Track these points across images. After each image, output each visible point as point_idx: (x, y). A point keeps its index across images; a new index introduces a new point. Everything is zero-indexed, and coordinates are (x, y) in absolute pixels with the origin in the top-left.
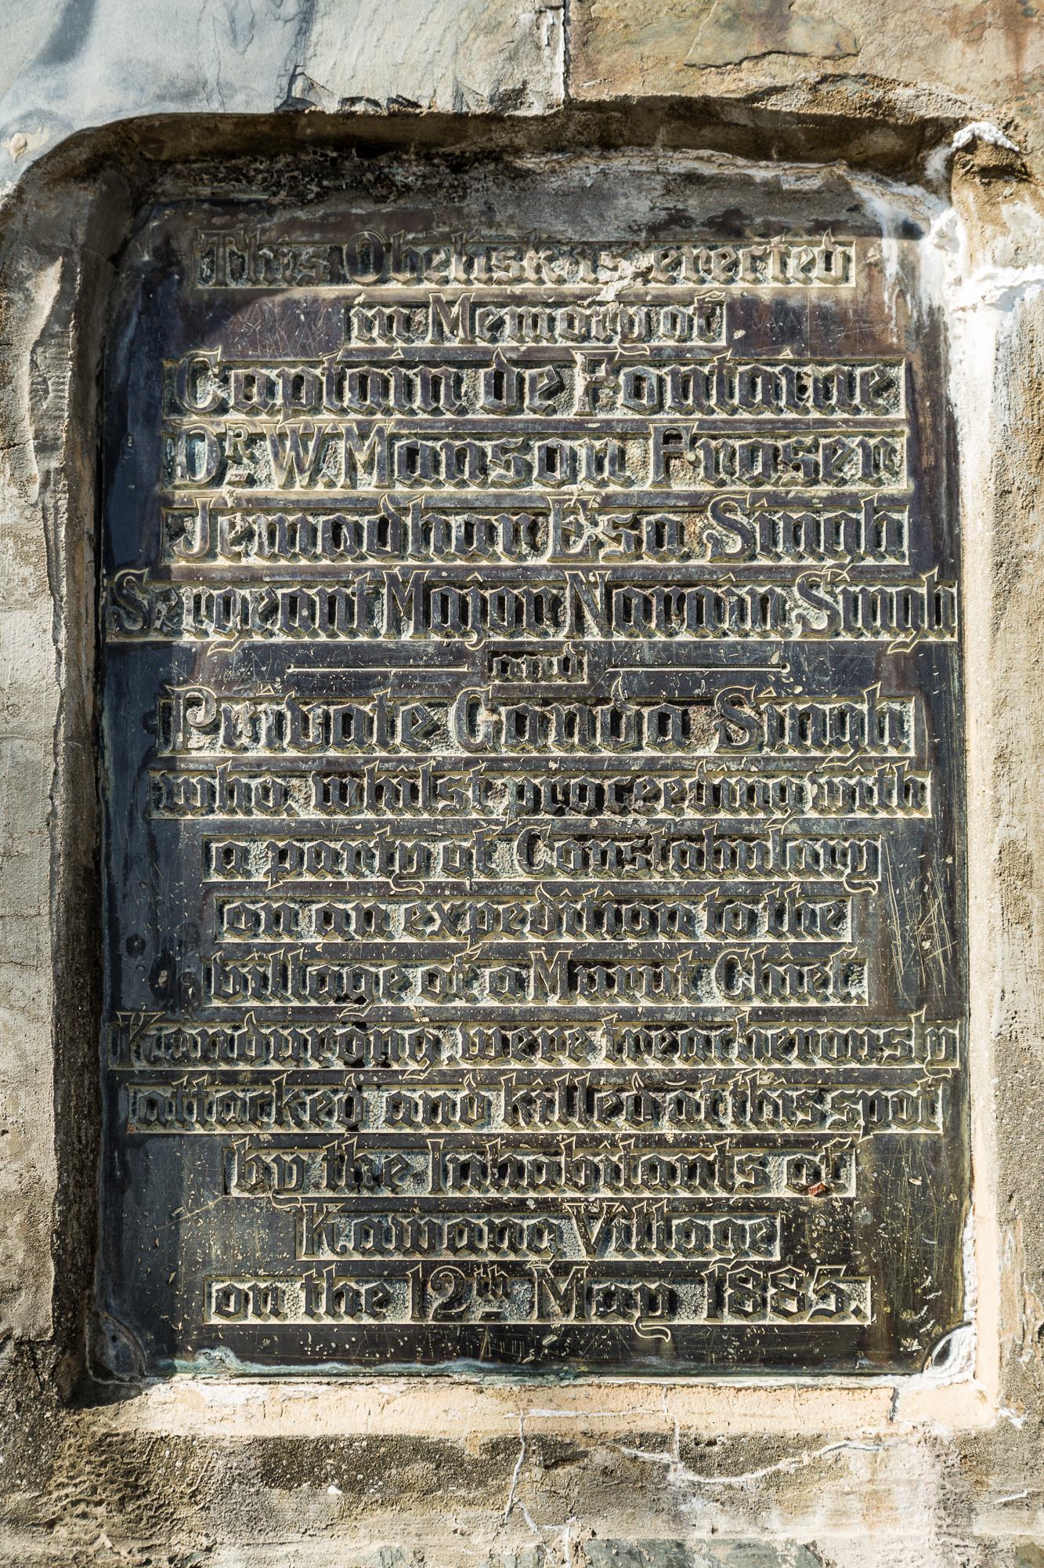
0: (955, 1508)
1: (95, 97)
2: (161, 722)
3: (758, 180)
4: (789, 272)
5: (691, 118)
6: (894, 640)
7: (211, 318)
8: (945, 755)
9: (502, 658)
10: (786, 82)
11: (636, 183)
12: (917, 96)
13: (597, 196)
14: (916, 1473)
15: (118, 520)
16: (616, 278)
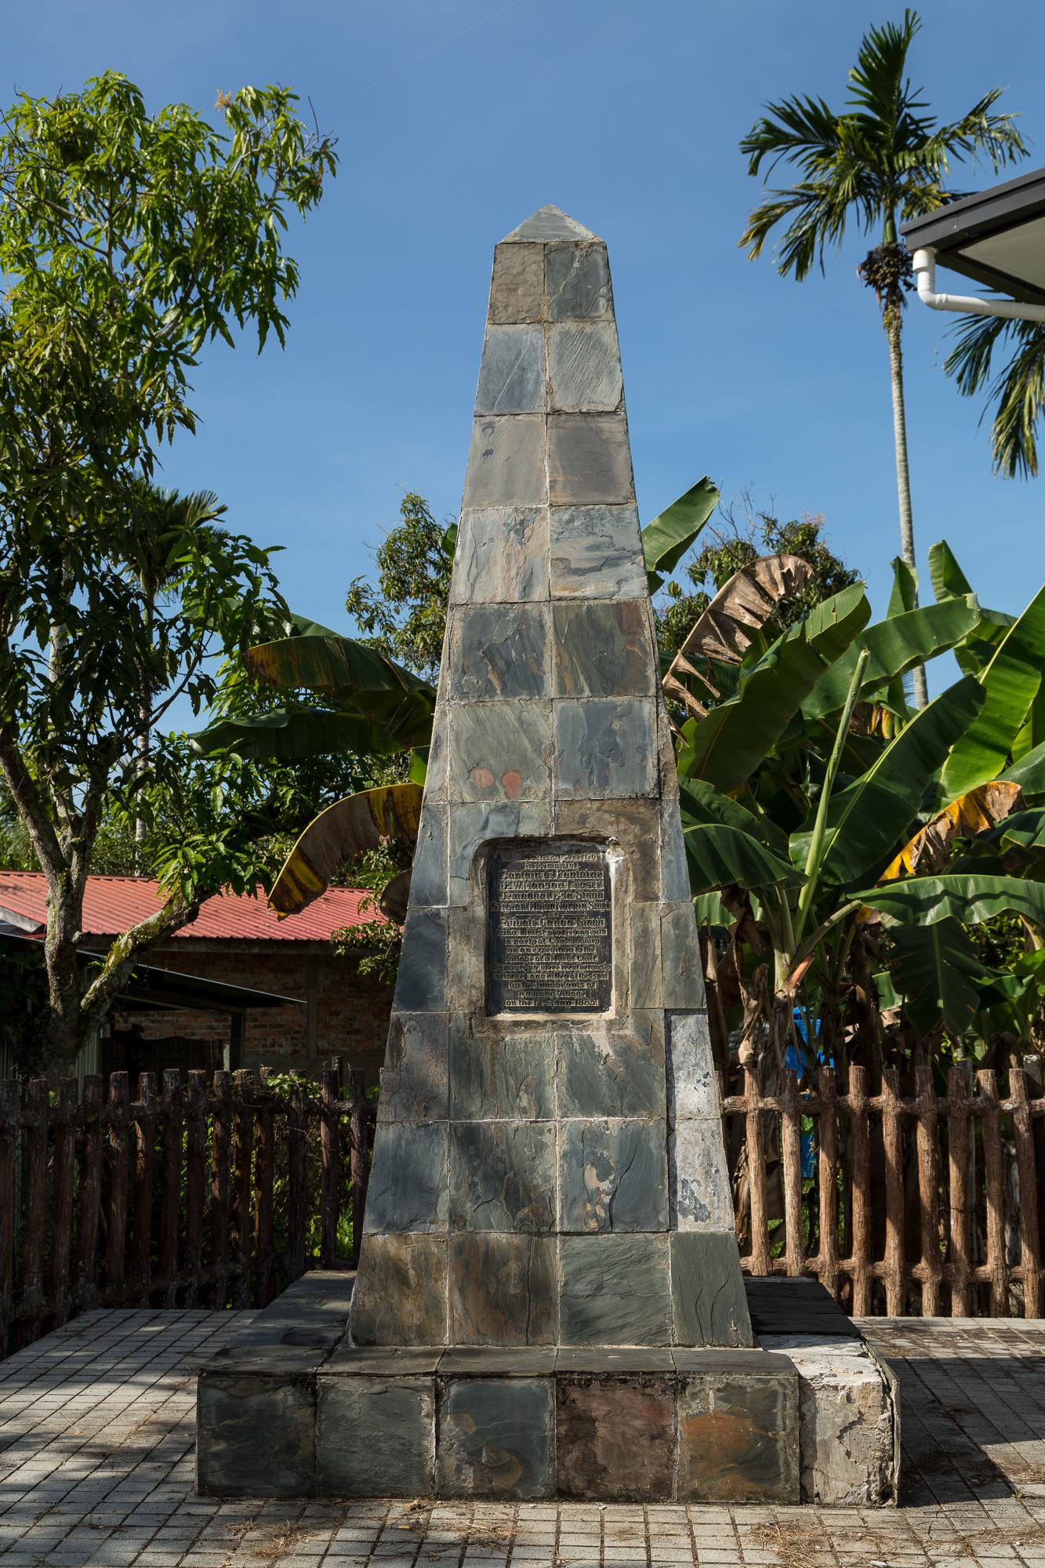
0: (609, 1030)
1: (489, 835)
2: (499, 922)
3: (425, 1443)
5: (573, 837)
6: (602, 910)
7: (504, 866)
8: (609, 926)
9: (546, 913)
10: (585, 831)
11: (565, 845)
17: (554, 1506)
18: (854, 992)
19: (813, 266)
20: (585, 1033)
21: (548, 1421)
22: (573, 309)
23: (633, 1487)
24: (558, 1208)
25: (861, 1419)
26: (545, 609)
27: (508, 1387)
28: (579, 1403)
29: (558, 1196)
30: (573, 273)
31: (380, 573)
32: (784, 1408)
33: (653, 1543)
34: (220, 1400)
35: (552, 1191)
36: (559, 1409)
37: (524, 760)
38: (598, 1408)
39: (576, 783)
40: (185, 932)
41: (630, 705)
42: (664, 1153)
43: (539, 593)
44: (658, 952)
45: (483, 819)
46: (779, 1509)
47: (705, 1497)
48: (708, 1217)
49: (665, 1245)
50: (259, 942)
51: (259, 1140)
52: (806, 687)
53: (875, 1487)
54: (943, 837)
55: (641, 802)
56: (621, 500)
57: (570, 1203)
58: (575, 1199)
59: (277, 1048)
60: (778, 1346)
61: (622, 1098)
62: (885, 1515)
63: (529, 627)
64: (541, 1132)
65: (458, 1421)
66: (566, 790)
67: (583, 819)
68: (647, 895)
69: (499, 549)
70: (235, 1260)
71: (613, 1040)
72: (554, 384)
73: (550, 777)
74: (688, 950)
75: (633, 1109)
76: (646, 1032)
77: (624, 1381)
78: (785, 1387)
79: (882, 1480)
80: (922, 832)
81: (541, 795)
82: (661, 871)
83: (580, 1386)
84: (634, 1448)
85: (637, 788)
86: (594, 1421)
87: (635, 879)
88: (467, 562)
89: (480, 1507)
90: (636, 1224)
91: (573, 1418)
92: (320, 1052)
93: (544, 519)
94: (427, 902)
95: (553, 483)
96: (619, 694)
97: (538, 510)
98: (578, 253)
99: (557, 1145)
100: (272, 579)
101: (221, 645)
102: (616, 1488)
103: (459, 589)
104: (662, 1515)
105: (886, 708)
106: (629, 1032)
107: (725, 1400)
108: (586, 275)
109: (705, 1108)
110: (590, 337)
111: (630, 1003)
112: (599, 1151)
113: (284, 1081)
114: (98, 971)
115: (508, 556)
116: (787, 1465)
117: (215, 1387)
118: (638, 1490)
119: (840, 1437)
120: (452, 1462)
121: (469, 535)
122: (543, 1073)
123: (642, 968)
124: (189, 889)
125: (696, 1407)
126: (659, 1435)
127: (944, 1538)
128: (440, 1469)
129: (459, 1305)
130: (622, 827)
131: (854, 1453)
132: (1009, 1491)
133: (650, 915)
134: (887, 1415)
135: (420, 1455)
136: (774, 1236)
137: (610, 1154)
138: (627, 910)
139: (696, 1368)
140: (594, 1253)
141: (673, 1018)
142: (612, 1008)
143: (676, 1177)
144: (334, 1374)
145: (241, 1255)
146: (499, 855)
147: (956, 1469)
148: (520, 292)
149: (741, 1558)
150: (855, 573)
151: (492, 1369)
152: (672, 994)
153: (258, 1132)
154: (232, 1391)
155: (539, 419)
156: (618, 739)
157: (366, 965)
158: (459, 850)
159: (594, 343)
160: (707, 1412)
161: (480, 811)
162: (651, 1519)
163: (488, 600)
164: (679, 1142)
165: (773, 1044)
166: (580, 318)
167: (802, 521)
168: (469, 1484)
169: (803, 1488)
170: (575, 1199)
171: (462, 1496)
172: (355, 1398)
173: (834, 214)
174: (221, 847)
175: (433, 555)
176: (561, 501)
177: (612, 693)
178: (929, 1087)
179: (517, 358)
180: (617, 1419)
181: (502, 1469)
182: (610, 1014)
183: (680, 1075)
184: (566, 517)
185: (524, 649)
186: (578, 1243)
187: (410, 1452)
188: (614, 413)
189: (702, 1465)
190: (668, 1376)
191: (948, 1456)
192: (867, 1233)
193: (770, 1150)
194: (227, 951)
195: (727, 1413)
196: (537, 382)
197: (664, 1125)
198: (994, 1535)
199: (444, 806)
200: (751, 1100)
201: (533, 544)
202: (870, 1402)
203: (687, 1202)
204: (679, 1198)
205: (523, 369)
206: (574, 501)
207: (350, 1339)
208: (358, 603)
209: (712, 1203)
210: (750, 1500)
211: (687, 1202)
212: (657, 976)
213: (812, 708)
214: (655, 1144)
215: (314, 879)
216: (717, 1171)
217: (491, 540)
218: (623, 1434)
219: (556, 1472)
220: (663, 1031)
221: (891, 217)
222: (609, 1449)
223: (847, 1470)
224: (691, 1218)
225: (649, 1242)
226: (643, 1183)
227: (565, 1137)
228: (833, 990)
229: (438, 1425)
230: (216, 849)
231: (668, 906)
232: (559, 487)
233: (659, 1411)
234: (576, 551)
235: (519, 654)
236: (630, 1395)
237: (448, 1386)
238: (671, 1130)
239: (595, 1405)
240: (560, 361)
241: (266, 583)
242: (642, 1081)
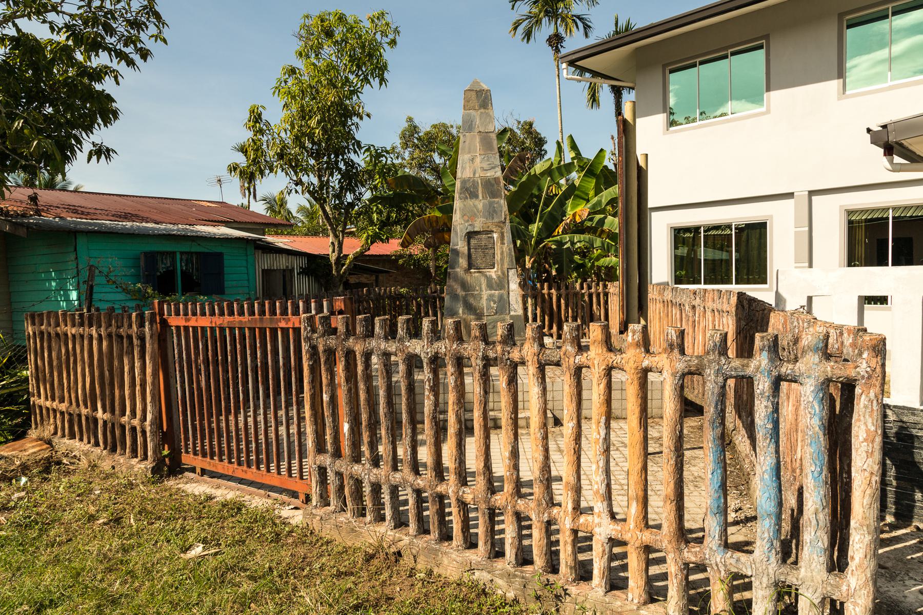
19: (532, 39)
40: (367, 253)
43: (477, 175)
57: (488, 309)
68: (503, 243)
69: (468, 165)
76: (503, 273)
90: (502, 313)
99: (485, 297)
103: (459, 175)
108: (486, 98)
114: (344, 265)
123: (502, 259)
133: (503, 248)
137: (496, 299)
146: (470, 235)
157: (401, 262)
159: (488, 115)
167: (528, 120)
173: (538, 22)
214: (505, 297)
221: (556, 24)
226: (503, 305)
228: (540, 264)
234: (486, 166)
242: (502, 283)
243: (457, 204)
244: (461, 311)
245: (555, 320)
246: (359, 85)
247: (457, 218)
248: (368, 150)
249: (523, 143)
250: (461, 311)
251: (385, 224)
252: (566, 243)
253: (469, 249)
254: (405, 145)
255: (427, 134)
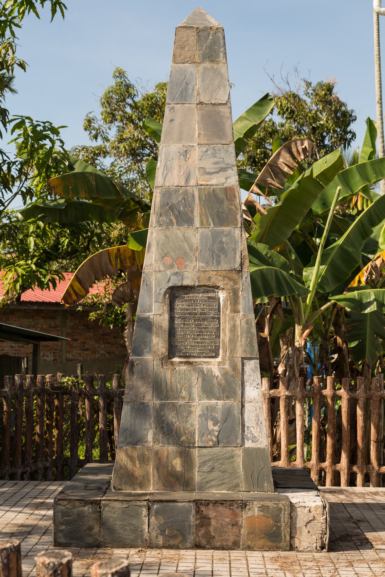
0: (219, 365)
1: (170, 284)
2: (174, 321)
3: (144, 527)
4: (211, 295)
5: (205, 286)
6: (217, 316)
7: (177, 297)
8: (219, 323)
10: (210, 284)
11: (202, 289)
12: (218, 285)
13: (199, 290)
14: (216, 363)
15: (172, 309)
16: (201, 295)
17: (194, 551)
18: (336, 339)
20: (209, 367)
21: (192, 519)
22: (209, 57)
23: (225, 544)
24: (197, 437)
25: (314, 519)
26: (195, 189)
27: (177, 506)
28: (204, 512)
29: (197, 432)
30: (209, 41)
31: (101, 109)
32: (284, 514)
33: (232, 562)
34: (62, 510)
35: (195, 430)
36: (196, 514)
37: (185, 253)
38: (211, 513)
39: (207, 263)
41: (230, 231)
42: (240, 416)
43: (192, 182)
44: (239, 334)
45: (168, 278)
46: (281, 552)
47: (253, 548)
48: (257, 441)
49: (239, 452)
50: (37, 303)
51: (57, 407)
52: (315, 197)
53: (319, 544)
54: (379, 266)
55: (234, 272)
56: (228, 143)
57: (202, 435)
58: (203, 434)
59: (45, 358)
60: (284, 492)
61: (223, 393)
62: (324, 553)
63: (188, 197)
64: (190, 406)
65: (157, 519)
66: (202, 266)
67: (210, 279)
68: (235, 311)
69: (176, 163)
70: (47, 460)
71: (220, 370)
72: (200, 91)
73: (196, 261)
74: (251, 333)
75: (228, 398)
76: (234, 367)
77: (222, 504)
78: (285, 506)
79: (321, 542)
80: (369, 264)
81: (192, 268)
82: (241, 301)
83: (205, 505)
84: (225, 529)
85: (232, 266)
86: (210, 519)
87: (231, 304)
88: (162, 168)
89: (165, 552)
90: (228, 444)
91: (201, 518)
92: (68, 360)
93: (195, 150)
94: (145, 312)
95: (199, 134)
96: (225, 226)
97: (192, 146)
98: (211, 32)
99: (197, 411)
100: (62, 142)
101: (36, 172)
102: (218, 544)
104: (235, 554)
105: (361, 194)
106: (227, 366)
107: (262, 511)
108: (215, 42)
109: (257, 398)
110: (216, 70)
111: (228, 355)
112: (214, 414)
113: (69, 380)
115: (180, 166)
116: (285, 536)
117: (60, 505)
118: (227, 545)
119: (306, 526)
120: (154, 534)
121: (163, 156)
122: (191, 383)
123: (233, 341)
124: (18, 287)
125: (250, 514)
126: (235, 524)
127: (343, 561)
128: (149, 537)
129: (156, 475)
130: (225, 282)
131: (311, 532)
132: (372, 547)
133: (236, 319)
134: (325, 517)
135: (141, 531)
136: (291, 453)
137: (219, 416)
138: (227, 316)
139: (251, 499)
140: (211, 455)
141: (245, 361)
142: (220, 357)
143: (244, 425)
144: (108, 500)
145: (49, 458)
146: (174, 293)
147: (353, 540)
148: (186, 49)
149: (265, 567)
150: (352, 111)
151: (170, 499)
152: (245, 351)
153: (56, 402)
154: (67, 506)
155: (194, 106)
156: (225, 245)
157: (93, 316)
158: (158, 290)
159: (217, 73)
160: (254, 516)
161: (167, 275)
162: (231, 555)
163: (171, 185)
164: (246, 411)
165: (293, 365)
166: (212, 61)
167: (326, 81)
168: (161, 542)
169: (291, 545)
170: (203, 434)
171: (158, 547)
172: (116, 509)
174: (34, 267)
175: (129, 101)
176: (202, 142)
177: (222, 226)
178: (363, 386)
179: (184, 79)
180: (219, 518)
181: (174, 537)
182: (219, 359)
183: (247, 384)
184: (204, 149)
185: (186, 206)
186: (205, 451)
187: (137, 530)
188: (226, 104)
189: (252, 536)
190: (239, 502)
191: (351, 536)
192: (333, 451)
193: (292, 413)
194: (20, 308)
195: (262, 516)
196: (193, 90)
197: (240, 404)
198: (363, 561)
199: (152, 272)
200: (282, 392)
201: (190, 161)
202: (318, 512)
203: (249, 435)
204: (246, 433)
205: (187, 84)
206: (208, 142)
207: (112, 488)
208: (90, 126)
209: (259, 436)
210: (270, 549)
211: (249, 435)
212: (239, 344)
213: (317, 208)
214: (236, 411)
215: (82, 289)
216: (261, 423)
217: (173, 159)
218: (221, 524)
219: (195, 538)
220: (241, 366)
222: (216, 529)
223: (309, 537)
224: (250, 441)
225: (233, 451)
226: (232, 427)
227: (200, 408)
229: (149, 520)
230: (32, 268)
231: (244, 315)
232: (202, 136)
233: (235, 515)
234: (209, 165)
235: (184, 208)
236: (224, 509)
237: (153, 505)
238: (243, 406)
239: (210, 513)
240: (203, 81)
241: (58, 143)
242: (231, 387)
243: (154, 234)
244: (150, 437)
245: (345, 445)
246: (15, 13)
247: (151, 260)
248: (18, 126)
249: (316, 119)
250: (150, 437)
251: (47, 257)
252: (370, 304)
253: (172, 319)
254: (111, 117)
255: (147, 98)
